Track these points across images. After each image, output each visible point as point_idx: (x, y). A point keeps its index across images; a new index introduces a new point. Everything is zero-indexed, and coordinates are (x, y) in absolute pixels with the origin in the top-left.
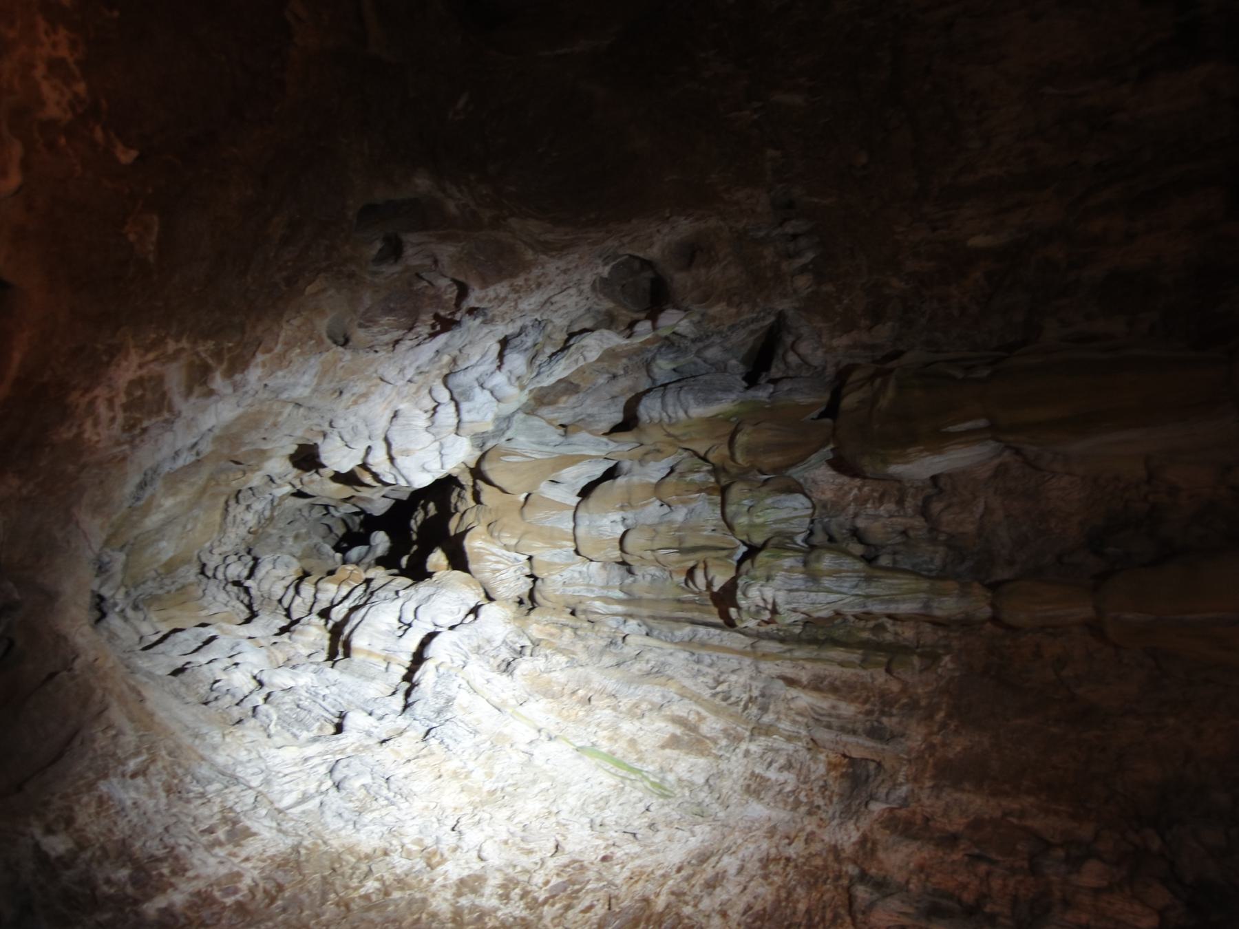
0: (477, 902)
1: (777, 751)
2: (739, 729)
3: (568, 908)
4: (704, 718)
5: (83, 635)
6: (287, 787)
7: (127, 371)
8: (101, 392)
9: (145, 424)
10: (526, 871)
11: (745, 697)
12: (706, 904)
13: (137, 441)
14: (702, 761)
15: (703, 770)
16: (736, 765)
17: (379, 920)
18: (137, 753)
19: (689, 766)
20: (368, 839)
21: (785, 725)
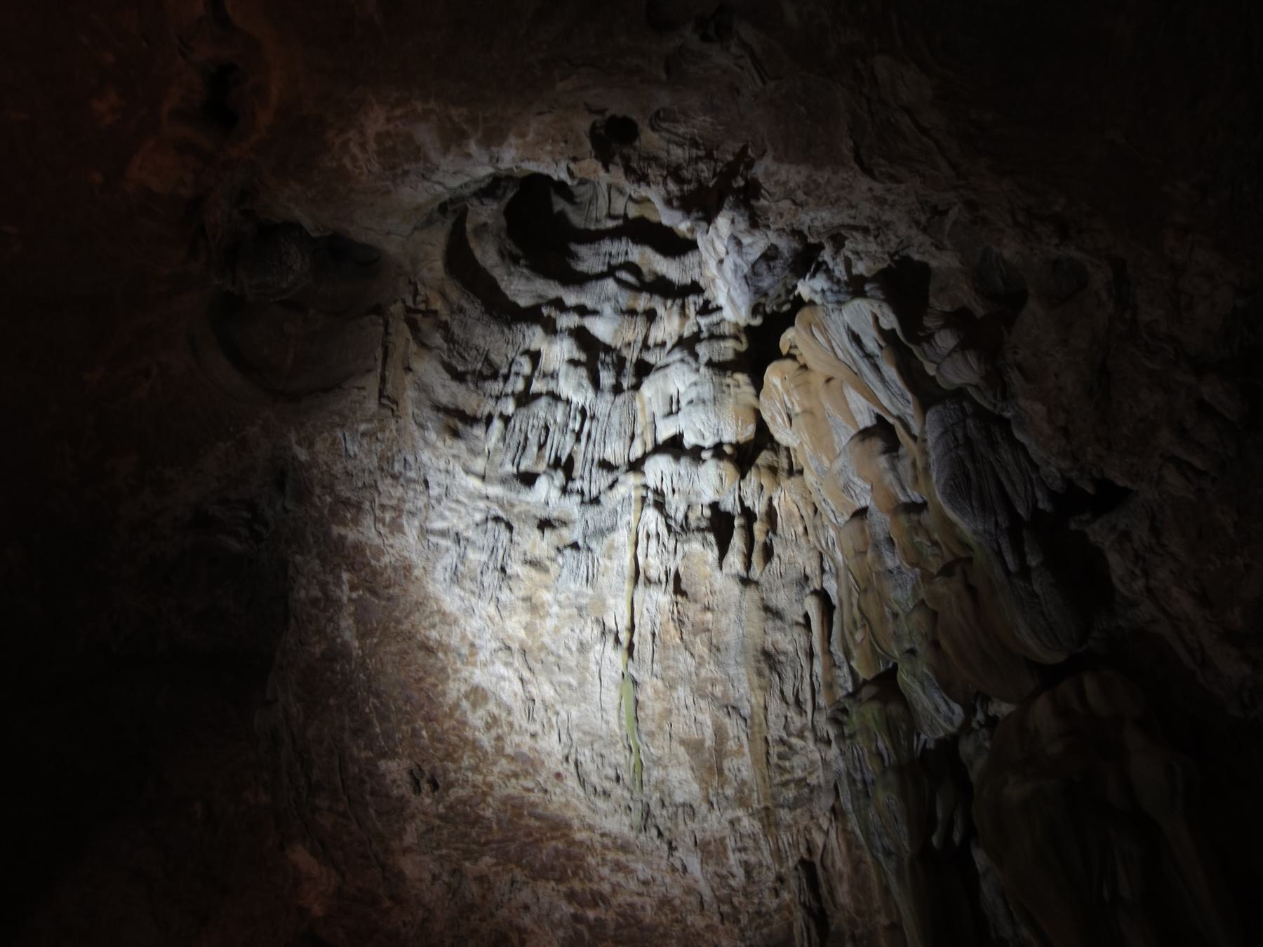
0: (469, 713)
1: (758, 848)
2: (755, 795)
3: (516, 775)
4: (743, 755)
5: (430, 270)
6: (447, 513)
7: (376, 121)
8: (352, 134)
9: (406, 167)
10: (511, 725)
11: (799, 773)
12: (605, 871)
13: (399, 181)
14: (695, 787)
15: (690, 793)
16: (714, 823)
17: (420, 661)
18: (370, 420)
19: (683, 781)
20: (451, 600)
21: (785, 838)
